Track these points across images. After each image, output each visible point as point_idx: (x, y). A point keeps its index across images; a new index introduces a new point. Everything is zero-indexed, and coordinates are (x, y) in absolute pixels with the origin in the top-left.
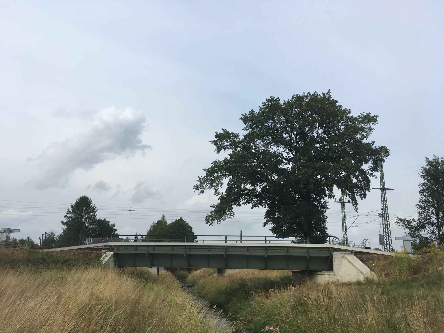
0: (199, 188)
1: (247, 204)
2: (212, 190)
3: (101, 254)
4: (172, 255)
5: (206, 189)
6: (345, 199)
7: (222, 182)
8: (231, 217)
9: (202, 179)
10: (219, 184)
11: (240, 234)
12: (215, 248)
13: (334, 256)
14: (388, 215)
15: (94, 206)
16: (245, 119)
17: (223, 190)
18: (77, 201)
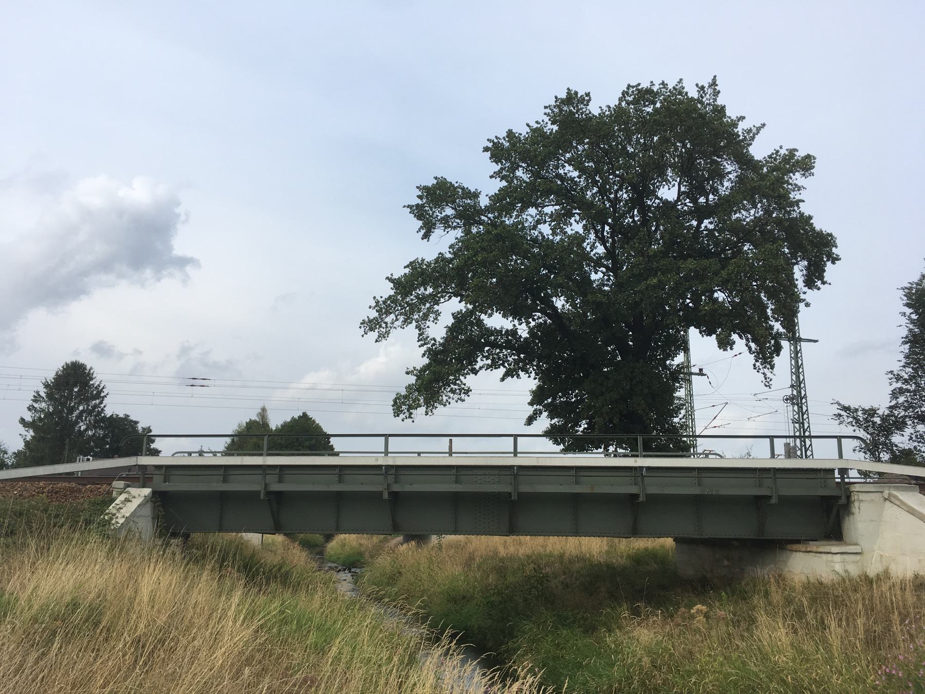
0: (375, 326)
1: (491, 370)
2: (411, 330)
3: (110, 493)
4: (339, 495)
5: (395, 328)
6: (694, 366)
7: (438, 310)
8: (463, 398)
9: (384, 302)
10: (431, 315)
11: (448, 448)
12: (475, 472)
13: (858, 496)
14: (806, 399)
15: (99, 386)
16: (496, 151)
17: (438, 331)
18: (57, 373)
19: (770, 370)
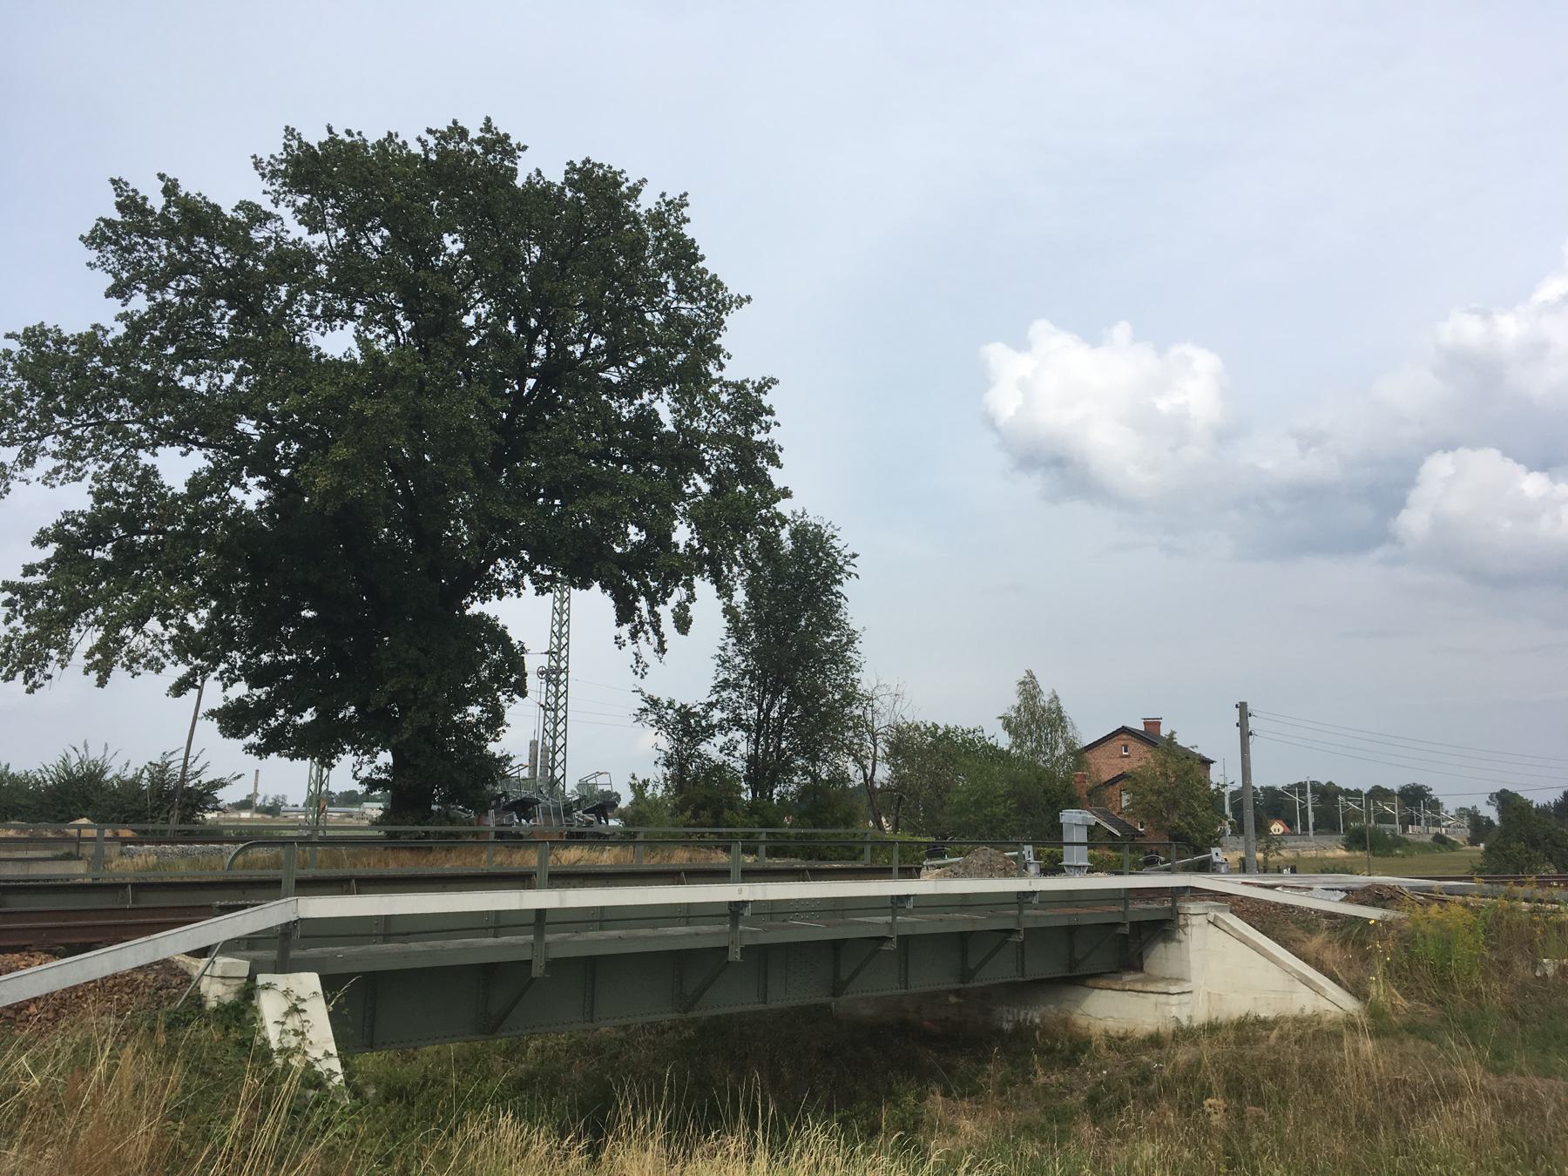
19: (660, 655)
